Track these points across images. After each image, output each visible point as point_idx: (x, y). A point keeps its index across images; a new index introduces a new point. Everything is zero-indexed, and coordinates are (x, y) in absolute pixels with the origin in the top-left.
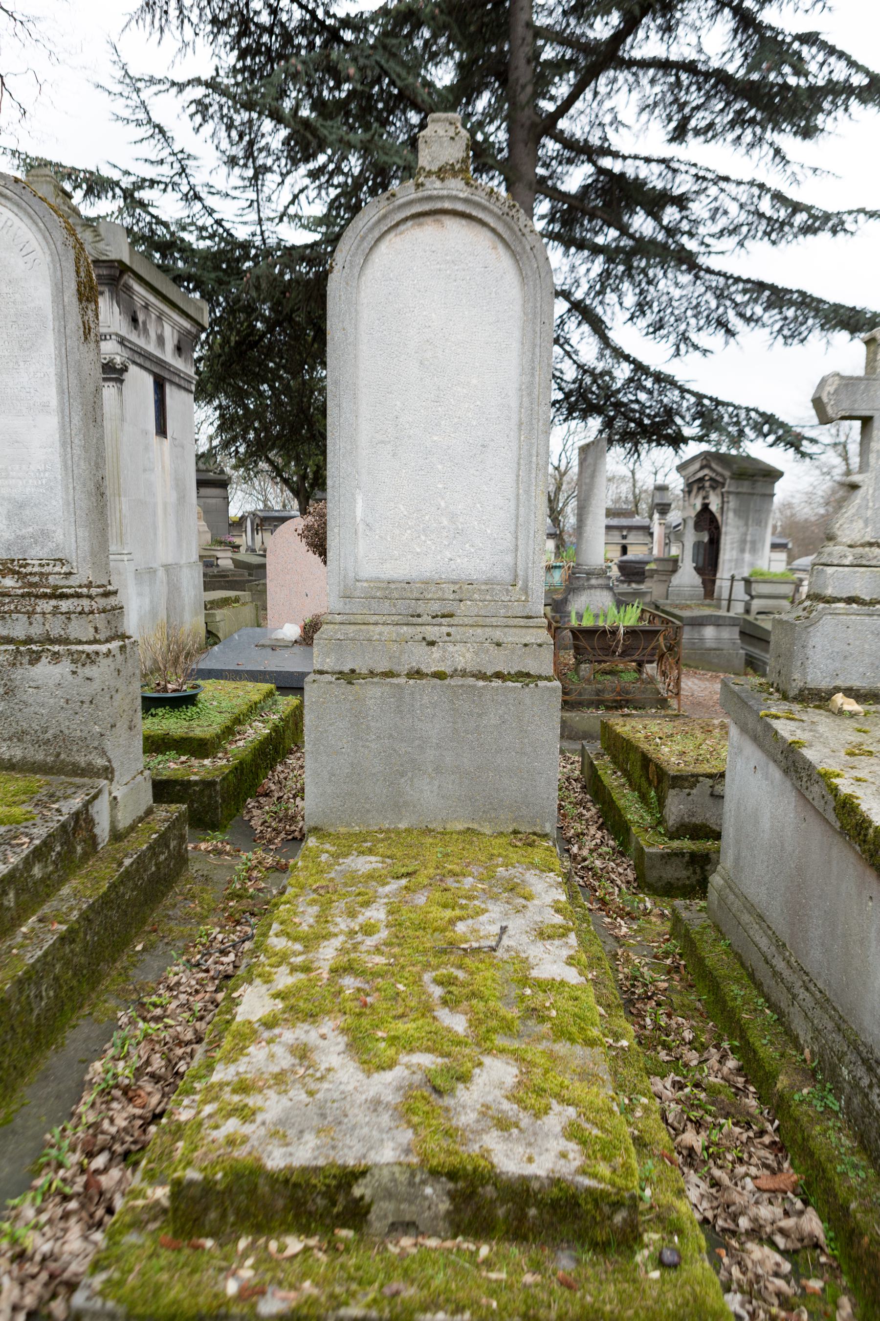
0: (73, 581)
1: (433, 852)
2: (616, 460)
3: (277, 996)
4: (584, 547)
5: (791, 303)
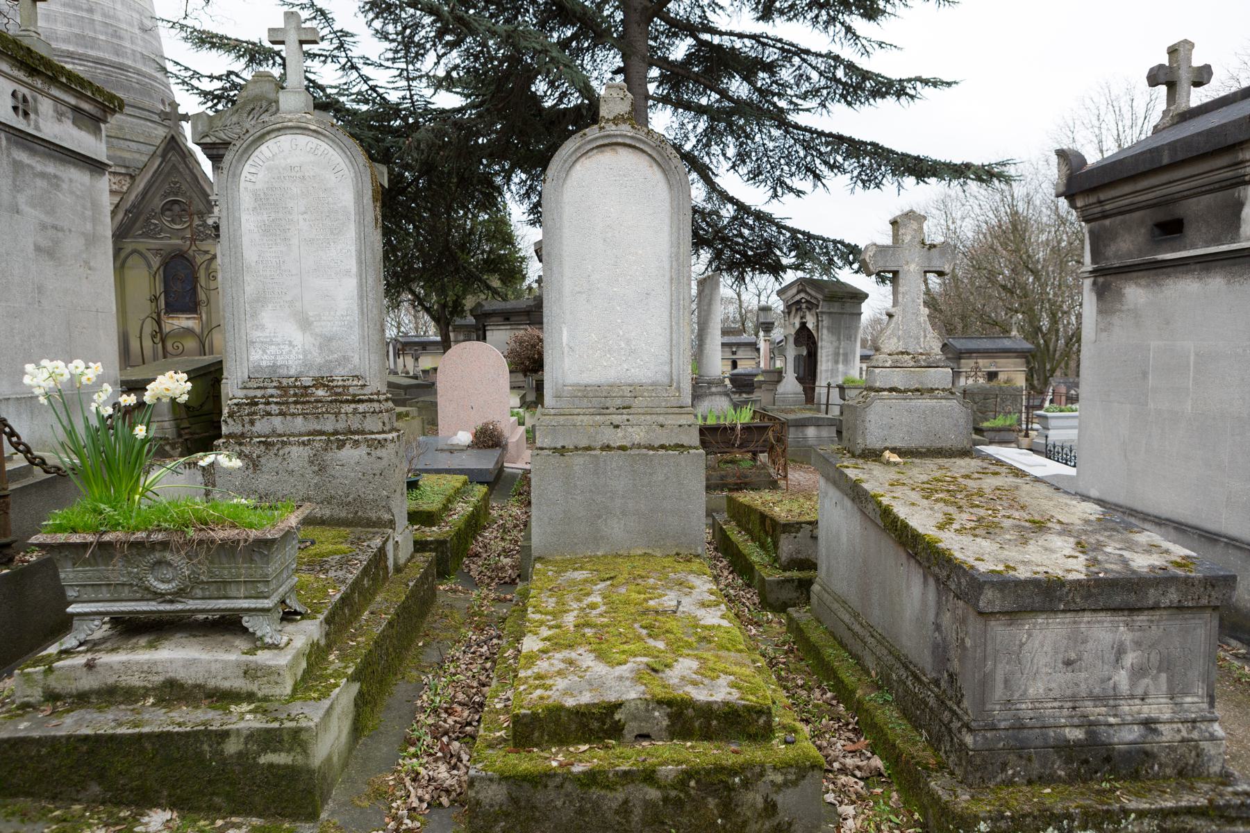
0: (367, 391)
1: (625, 567)
2: (726, 286)
3: (544, 639)
4: (704, 361)
5: (867, 153)
